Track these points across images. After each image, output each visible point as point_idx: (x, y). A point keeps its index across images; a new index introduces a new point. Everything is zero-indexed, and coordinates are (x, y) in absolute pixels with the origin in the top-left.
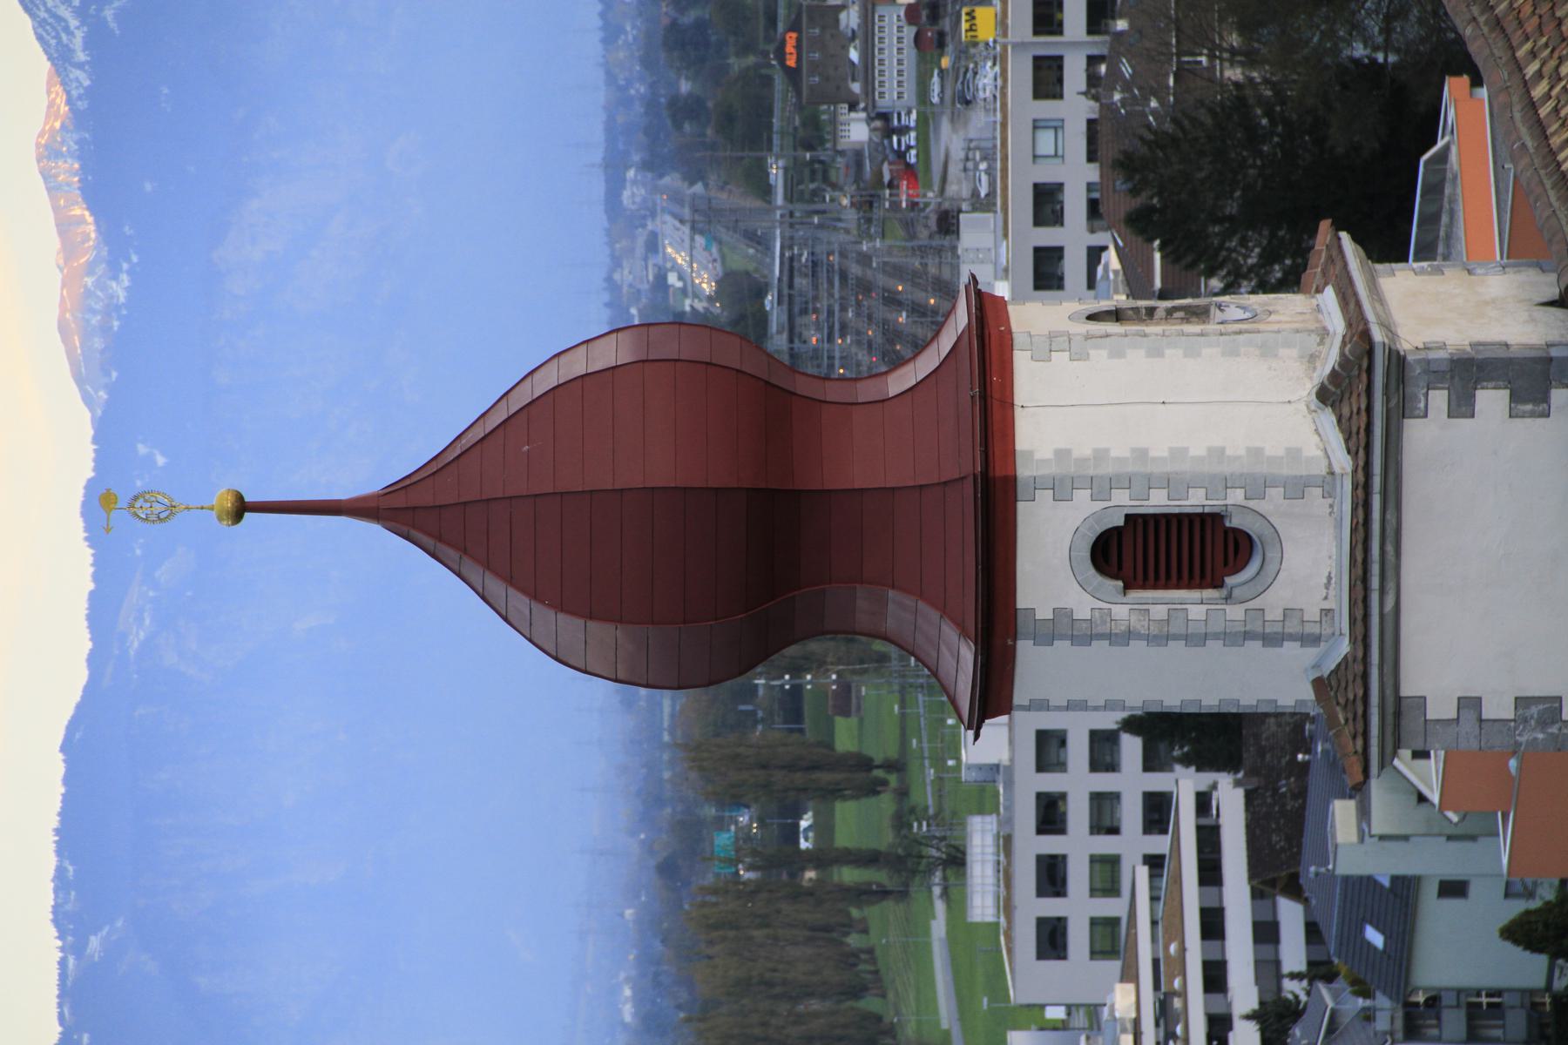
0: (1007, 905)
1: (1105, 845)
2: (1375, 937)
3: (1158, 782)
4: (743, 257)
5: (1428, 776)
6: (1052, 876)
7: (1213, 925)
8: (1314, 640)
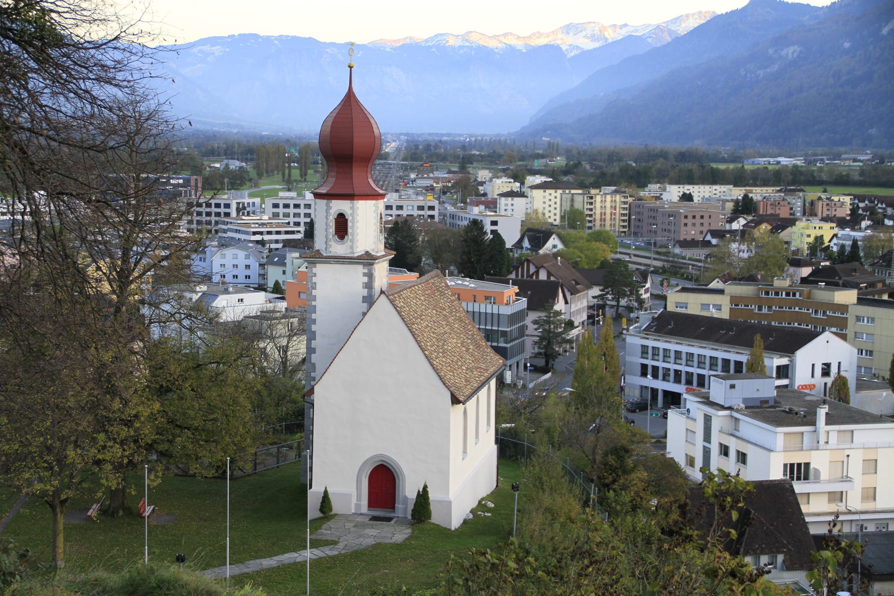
0: (281, 198)
1: (292, 215)
2: (276, 259)
3: (302, 224)
4: (392, 156)
5: (303, 269)
6: (286, 206)
7: (278, 233)
8: (326, 249)
